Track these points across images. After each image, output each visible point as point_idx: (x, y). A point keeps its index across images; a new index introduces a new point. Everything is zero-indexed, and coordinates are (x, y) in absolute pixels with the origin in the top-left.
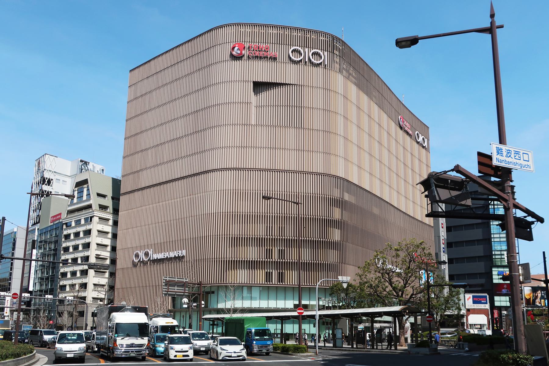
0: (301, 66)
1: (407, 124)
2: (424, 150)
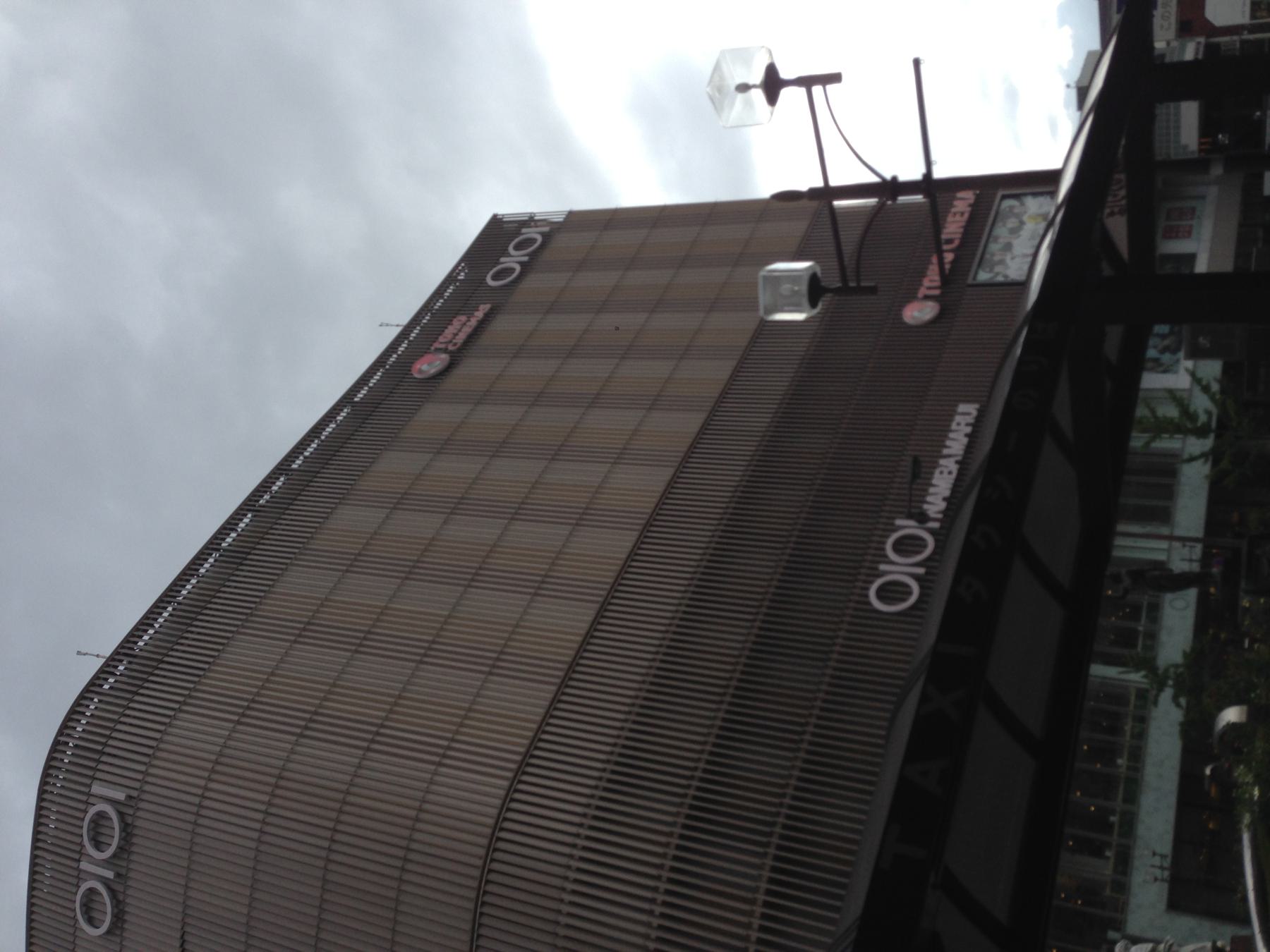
1: (450, 331)
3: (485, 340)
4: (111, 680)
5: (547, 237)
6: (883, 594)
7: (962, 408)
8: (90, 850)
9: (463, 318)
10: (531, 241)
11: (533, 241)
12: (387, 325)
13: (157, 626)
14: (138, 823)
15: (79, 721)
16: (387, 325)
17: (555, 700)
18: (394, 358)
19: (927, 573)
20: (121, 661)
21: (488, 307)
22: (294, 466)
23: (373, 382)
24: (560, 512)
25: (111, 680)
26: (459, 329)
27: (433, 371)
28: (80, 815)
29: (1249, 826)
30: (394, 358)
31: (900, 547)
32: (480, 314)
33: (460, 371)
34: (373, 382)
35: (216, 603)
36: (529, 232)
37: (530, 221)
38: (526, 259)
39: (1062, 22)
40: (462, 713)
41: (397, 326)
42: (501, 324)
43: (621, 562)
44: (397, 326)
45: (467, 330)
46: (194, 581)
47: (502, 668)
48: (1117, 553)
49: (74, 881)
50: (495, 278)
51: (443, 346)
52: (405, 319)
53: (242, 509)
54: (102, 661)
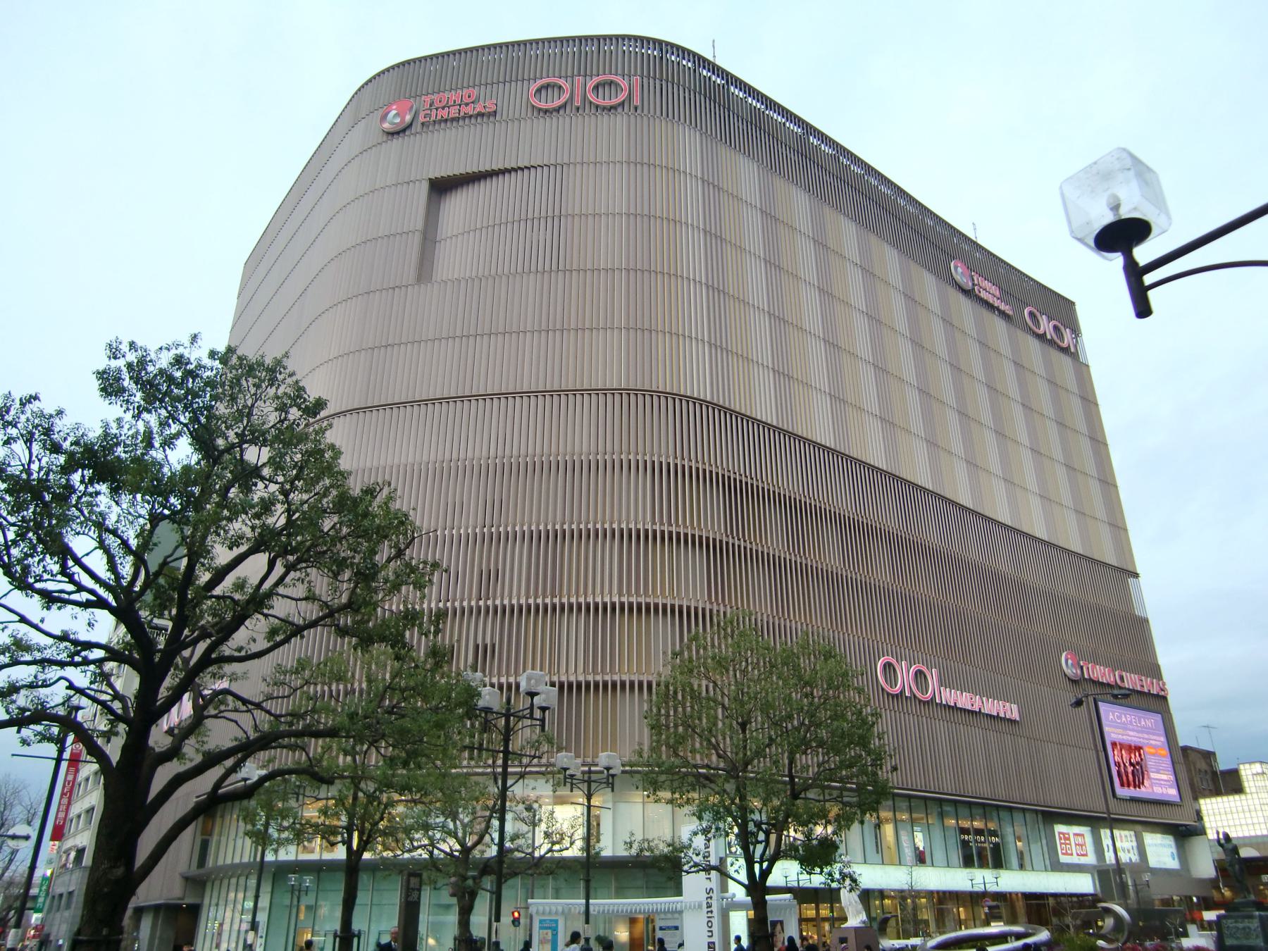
0: (562, 121)
1: (986, 284)
2: (1066, 360)
3: (986, 313)
4: (690, 65)
5: (1065, 350)
6: (888, 667)
7: (1014, 707)
8: (591, 84)
9: (997, 293)
10: (1061, 337)
11: (1062, 339)
12: (975, 229)
13: (767, 112)
14: (619, 117)
15: (689, 61)
16: (975, 229)
17: (702, 402)
18: (873, 182)
19: (906, 697)
20: (723, 79)
21: (1011, 313)
22: (732, 89)
23: (882, 188)
24: (783, 359)
25: (690, 65)
26: (989, 291)
27: (958, 278)
28: (613, 72)
29: (1225, 886)
30: (873, 182)
31: (919, 674)
32: (1003, 307)
33: (962, 298)
34: (882, 188)
35: (720, 110)
36: (1067, 334)
37: (1076, 331)
38: (1049, 337)
39: (62, 631)
40: (724, 346)
41: (714, 56)
42: (1000, 324)
43: (727, 405)
44: (714, 56)
45: (991, 299)
46: (741, 95)
47: (784, 381)
48: (1102, 831)
49: (563, 74)
50: (1031, 314)
51: (976, 282)
52: (979, 242)
53: (727, 76)
54: (711, 59)
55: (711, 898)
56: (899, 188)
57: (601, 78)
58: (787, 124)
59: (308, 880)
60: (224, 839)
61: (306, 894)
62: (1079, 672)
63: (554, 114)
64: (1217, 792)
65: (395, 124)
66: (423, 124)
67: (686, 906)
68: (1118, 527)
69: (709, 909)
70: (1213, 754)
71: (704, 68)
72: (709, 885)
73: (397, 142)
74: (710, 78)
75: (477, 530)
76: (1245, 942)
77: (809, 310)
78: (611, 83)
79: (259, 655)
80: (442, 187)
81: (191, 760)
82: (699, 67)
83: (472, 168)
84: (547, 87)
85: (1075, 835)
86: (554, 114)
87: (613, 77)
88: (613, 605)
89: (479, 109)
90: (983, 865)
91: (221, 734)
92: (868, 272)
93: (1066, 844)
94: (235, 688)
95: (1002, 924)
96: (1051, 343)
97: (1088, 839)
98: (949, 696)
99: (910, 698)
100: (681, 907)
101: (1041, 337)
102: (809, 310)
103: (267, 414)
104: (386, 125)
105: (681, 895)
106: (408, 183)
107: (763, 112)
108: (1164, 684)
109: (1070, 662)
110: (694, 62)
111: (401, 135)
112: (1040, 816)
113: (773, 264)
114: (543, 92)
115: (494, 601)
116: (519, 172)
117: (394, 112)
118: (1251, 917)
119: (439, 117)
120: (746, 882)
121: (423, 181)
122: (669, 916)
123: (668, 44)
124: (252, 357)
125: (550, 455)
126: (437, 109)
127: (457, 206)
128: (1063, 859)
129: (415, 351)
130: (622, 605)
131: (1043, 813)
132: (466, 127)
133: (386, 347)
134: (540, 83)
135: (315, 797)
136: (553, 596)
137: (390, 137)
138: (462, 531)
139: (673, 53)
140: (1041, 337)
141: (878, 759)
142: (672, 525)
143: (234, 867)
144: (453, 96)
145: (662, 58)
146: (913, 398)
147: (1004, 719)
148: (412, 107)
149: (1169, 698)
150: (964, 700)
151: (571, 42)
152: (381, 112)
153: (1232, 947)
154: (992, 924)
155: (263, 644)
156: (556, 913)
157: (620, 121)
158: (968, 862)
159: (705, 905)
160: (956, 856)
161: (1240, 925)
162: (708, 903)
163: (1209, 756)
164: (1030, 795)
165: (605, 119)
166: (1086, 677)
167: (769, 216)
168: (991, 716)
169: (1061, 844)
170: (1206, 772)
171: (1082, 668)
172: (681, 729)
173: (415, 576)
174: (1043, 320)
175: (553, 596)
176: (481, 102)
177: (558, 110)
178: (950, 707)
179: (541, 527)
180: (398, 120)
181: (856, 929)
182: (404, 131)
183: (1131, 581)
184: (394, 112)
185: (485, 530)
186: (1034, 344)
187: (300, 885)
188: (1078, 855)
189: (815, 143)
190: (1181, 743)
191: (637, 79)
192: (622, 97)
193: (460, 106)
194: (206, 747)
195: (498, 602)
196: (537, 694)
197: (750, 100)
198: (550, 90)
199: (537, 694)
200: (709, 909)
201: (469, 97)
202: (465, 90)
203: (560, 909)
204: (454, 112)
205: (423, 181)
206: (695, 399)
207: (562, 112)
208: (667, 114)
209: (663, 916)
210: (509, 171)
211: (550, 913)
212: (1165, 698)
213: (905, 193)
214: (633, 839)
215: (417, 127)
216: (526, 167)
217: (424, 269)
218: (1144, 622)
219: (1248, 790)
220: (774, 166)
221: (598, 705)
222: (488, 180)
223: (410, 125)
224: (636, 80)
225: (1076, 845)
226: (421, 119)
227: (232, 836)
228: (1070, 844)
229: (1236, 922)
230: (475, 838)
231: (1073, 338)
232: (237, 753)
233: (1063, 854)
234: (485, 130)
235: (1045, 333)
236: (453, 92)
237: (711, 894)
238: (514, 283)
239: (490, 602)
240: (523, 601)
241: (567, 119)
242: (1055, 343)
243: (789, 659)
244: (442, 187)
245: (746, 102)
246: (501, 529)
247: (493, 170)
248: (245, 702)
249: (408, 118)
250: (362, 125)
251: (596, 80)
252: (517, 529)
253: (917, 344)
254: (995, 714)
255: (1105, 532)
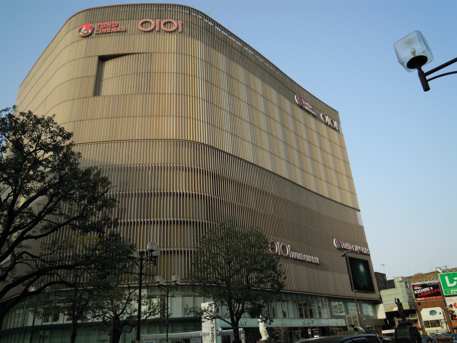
0: (151, 36)
2: (335, 133)
3: (307, 115)
4: (201, 17)
5: (335, 129)
8: (162, 22)
15: (200, 16)
32: (313, 113)
34: (271, 67)
36: (335, 123)
37: (339, 123)
38: (329, 124)
42: (312, 120)
55: (213, 330)
56: (277, 68)
57: (166, 20)
58: (236, 42)
59: (47, 333)
60: (9, 319)
61: (47, 339)
62: (340, 246)
63: (148, 33)
64: (386, 288)
65: (84, 33)
66: (96, 34)
67: (203, 334)
68: (353, 193)
69: (213, 335)
70: (385, 275)
71: (206, 19)
72: (212, 326)
73: (85, 40)
74: (208, 23)
75: (117, 193)
76: (404, 337)
77: (244, 110)
78: (170, 22)
79: (36, 238)
80: (103, 59)
81: (8, 282)
82: (204, 18)
83: (116, 52)
84: (145, 22)
85: (339, 305)
86: (148, 33)
87: (171, 20)
88: (171, 221)
89: (118, 29)
90: (307, 317)
91: (21, 270)
92: (265, 98)
93: (335, 308)
94: (28, 251)
95: (318, 336)
96: (330, 126)
97: (343, 306)
98: (294, 255)
99: (280, 256)
100: (202, 334)
101: (327, 124)
102: (244, 110)
103: (45, 138)
104: (81, 34)
105: (201, 330)
106: (90, 57)
107: (228, 37)
108: (369, 250)
109: (337, 242)
110: (202, 16)
111: (89, 37)
112: (327, 299)
113: (231, 94)
114: (144, 25)
115: (124, 220)
116: (129, 55)
117: (84, 29)
118: (407, 328)
119: (102, 32)
120: (231, 322)
121: (96, 57)
122: (195, 339)
123: (192, 9)
124: (39, 116)
125: (143, 164)
126: (101, 28)
127: (109, 65)
128: (335, 314)
129: (90, 122)
130: (174, 221)
131: (328, 297)
132: (113, 36)
133: (81, 121)
134: (142, 21)
135: (59, 296)
136: (147, 218)
137: (82, 38)
138: (111, 193)
139: (194, 13)
140: (327, 124)
141: (279, 275)
142: (193, 191)
143: (14, 329)
144: (109, 23)
145: (190, 14)
146: (281, 145)
147: (314, 263)
148: (92, 27)
149: (370, 254)
150: (299, 256)
151: (155, 6)
152: (78, 29)
153: (400, 339)
154: (315, 336)
155: (38, 233)
156: (153, 339)
157: (174, 37)
158: (301, 316)
159: (211, 333)
160: (297, 313)
161: (403, 331)
162: (212, 333)
163: (383, 275)
164: (324, 291)
165: (168, 36)
166: (342, 247)
167: (230, 76)
168: (309, 262)
169: (334, 308)
170: (382, 281)
171: (341, 244)
172: (205, 265)
173: (109, 203)
174: (327, 118)
175: (147, 218)
176: (119, 27)
177: (150, 32)
178: (295, 259)
179: (143, 192)
180: (86, 32)
181: (265, 341)
182: (88, 36)
183: (358, 213)
184: (84, 29)
185: (121, 193)
186: (324, 126)
187: (44, 335)
188: (340, 312)
189: (246, 50)
190: (375, 271)
191: (180, 22)
192: (174, 28)
193: (111, 28)
194: (15, 276)
195: (126, 221)
196: (154, 251)
197: (223, 32)
198: (146, 23)
199: (154, 251)
200: (213, 335)
201: (115, 24)
202: (110, 22)
203: (154, 338)
204: (108, 30)
205: (96, 57)
206: (202, 143)
207: (151, 33)
208: (191, 35)
209: (193, 339)
210: (131, 54)
211: (148, 339)
212: (369, 255)
213: (279, 69)
214: (187, 307)
215: (94, 35)
216: (140, 53)
217: (97, 91)
218: (362, 227)
219: (397, 287)
220: (231, 58)
221: (165, 259)
222: (120, 58)
223: (91, 35)
224: (180, 22)
225: (339, 309)
226: (95, 32)
227: (13, 317)
228: (337, 308)
229: (401, 330)
230: (121, 311)
231: (337, 125)
232: (34, 276)
233: (334, 312)
234: (121, 38)
235: (328, 123)
236: (108, 22)
237: (213, 329)
238: (83, 124)
239: (122, 221)
240: (135, 220)
241: (153, 35)
242: (331, 126)
243: (246, 236)
244: (103, 59)
245: (221, 33)
246: (127, 192)
247: (124, 54)
248: (32, 256)
249: (90, 31)
250: (70, 33)
251: (164, 21)
252: (133, 192)
253: (283, 125)
254: (310, 261)
255: (348, 195)
